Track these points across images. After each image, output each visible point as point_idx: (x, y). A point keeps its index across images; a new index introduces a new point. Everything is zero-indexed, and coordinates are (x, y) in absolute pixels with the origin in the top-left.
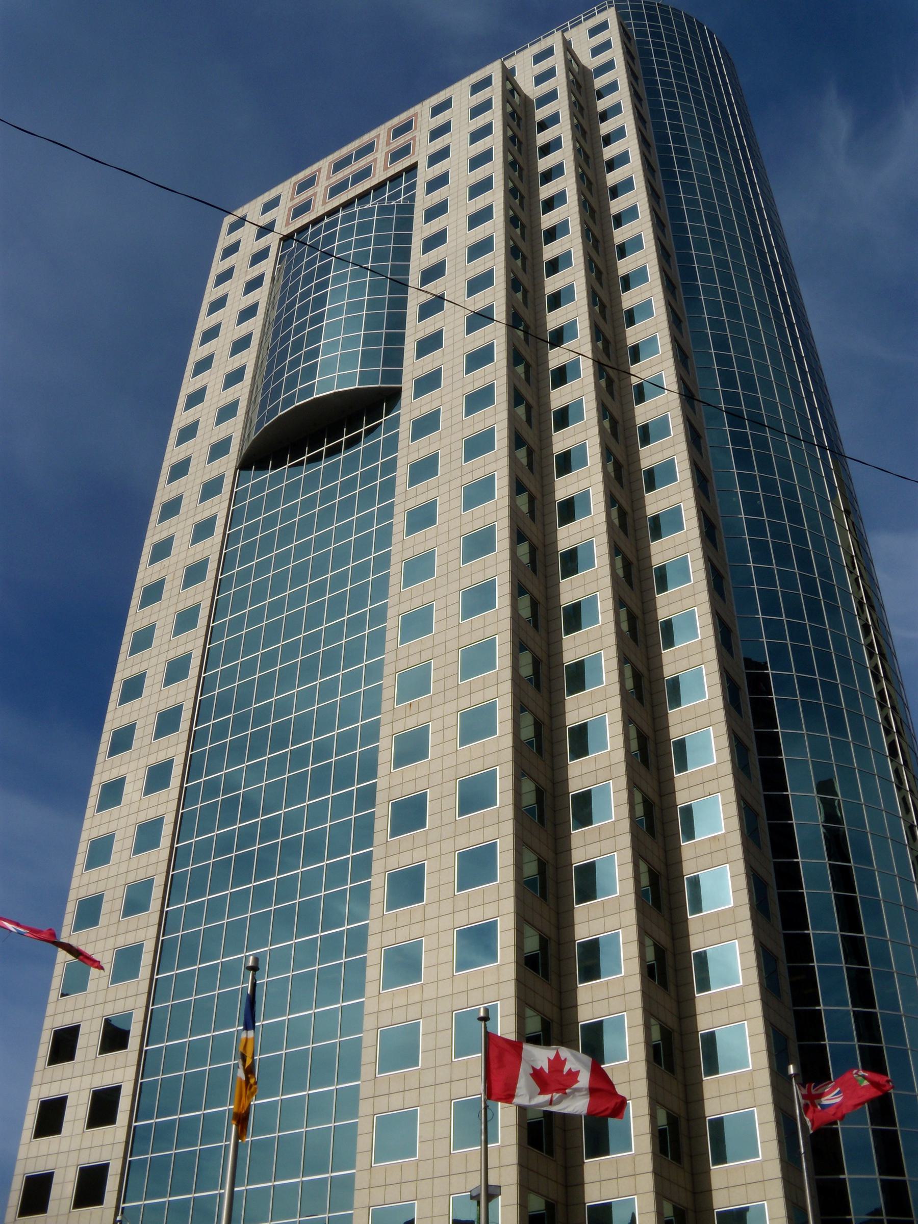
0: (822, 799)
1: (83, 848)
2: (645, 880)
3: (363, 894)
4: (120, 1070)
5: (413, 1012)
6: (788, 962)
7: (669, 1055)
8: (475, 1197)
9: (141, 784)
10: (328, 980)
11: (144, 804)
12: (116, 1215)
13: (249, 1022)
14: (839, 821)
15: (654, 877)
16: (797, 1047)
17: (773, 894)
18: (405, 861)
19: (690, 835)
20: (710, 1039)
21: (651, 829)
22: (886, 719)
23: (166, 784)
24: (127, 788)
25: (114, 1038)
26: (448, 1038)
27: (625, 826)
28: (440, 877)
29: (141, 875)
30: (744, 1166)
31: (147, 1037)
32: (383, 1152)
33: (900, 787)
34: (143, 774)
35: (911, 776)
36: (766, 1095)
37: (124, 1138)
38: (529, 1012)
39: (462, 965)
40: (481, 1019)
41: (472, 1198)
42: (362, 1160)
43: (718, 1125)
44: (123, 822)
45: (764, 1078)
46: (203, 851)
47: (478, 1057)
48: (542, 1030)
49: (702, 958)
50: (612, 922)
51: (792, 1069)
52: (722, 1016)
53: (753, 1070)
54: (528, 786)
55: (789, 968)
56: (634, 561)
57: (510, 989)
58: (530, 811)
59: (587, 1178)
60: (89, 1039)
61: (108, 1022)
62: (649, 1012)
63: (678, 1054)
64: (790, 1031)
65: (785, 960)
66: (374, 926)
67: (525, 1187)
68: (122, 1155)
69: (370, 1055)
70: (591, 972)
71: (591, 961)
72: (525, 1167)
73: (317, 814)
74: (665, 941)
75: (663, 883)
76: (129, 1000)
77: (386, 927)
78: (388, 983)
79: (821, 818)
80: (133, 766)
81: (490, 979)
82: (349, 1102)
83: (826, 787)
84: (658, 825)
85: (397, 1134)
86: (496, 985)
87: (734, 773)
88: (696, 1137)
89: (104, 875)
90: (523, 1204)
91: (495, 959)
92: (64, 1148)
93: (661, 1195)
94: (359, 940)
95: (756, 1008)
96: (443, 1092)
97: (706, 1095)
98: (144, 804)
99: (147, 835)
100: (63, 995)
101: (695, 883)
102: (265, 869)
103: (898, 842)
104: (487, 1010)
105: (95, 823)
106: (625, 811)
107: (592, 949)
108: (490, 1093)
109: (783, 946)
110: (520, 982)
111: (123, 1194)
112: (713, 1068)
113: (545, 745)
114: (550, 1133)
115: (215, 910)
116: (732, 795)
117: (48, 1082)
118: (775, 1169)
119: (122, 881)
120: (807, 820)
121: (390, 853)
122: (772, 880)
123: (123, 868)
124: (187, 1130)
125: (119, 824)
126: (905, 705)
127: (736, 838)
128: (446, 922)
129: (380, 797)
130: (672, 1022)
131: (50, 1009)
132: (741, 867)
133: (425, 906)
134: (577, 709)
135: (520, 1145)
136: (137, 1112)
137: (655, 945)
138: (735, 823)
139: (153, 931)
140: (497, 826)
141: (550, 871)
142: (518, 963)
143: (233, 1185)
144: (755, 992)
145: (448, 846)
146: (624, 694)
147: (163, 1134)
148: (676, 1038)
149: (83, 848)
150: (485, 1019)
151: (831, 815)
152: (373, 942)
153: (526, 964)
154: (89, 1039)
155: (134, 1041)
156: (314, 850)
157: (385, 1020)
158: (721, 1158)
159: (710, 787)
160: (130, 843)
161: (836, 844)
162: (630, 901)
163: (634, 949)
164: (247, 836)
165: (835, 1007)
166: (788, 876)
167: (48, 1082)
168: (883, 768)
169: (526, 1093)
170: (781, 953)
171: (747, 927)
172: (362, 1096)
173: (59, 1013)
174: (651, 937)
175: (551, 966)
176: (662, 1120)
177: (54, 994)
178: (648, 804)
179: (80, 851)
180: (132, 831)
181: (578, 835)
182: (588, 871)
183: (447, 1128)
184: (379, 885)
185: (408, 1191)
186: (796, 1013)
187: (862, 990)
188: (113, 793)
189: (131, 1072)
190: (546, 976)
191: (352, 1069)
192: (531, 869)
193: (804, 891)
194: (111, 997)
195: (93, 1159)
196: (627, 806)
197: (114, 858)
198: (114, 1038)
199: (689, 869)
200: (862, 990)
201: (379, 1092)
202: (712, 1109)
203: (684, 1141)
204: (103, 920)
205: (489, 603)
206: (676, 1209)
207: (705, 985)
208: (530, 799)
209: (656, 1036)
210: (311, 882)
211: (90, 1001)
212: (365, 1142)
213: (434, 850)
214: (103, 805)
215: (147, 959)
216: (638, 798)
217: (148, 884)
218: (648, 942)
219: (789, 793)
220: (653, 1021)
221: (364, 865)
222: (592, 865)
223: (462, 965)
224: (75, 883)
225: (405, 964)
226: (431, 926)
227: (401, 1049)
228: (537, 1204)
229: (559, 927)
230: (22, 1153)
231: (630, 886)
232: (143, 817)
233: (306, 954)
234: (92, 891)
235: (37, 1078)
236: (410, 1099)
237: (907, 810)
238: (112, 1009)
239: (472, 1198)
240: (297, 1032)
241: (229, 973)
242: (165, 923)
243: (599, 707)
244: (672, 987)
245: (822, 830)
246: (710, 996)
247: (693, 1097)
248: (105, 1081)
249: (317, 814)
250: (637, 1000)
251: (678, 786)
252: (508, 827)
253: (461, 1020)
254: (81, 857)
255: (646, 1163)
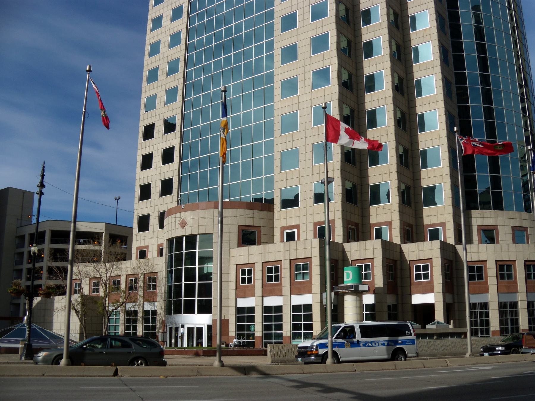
0: (474, 13)
1: (145, 74)
2: (394, 48)
3: (271, 57)
4: (173, 140)
5: (295, 108)
6: (456, 84)
7: (404, 123)
8: (323, 183)
9: (170, 17)
10: (258, 96)
11: (172, 26)
12: (178, 198)
13: (225, 114)
14: (482, 24)
15: (398, 47)
16: (458, 118)
17: (451, 55)
18: (288, 43)
19: (414, 28)
20: (422, 117)
21: (397, 26)
22: (526, 123)
23: (181, 16)
24: (164, 20)
25: (169, 127)
26: (310, 118)
27: (385, 24)
28: (304, 49)
29: (174, 57)
30: (434, 169)
31: (183, 126)
32: (285, 166)
33: (510, 9)
34: (170, 13)
35: (515, 4)
36: (445, 140)
37: (178, 167)
38: (344, 106)
39: (315, 86)
40: (323, 108)
41: (322, 183)
42: (276, 170)
43: (424, 152)
44: (163, 35)
45: (444, 133)
46: (200, 44)
47: (322, 126)
48: (346, 15)
49: (419, 82)
50: (380, 67)
51: (455, 129)
52: (426, 107)
53: (433, 60)
54: (342, 7)
55: (456, 87)
56: (400, 13)
57: (336, 96)
58: (343, 18)
59: (370, 174)
60: (159, 129)
61: (166, 121)
62: (396, 105)
63: (408, 123)
64: (456, 114)
65: (448, 20)
66: (276, 71)
67: (344, 179)
68: (186, 26)
69: (277, 127)
70: (371, 88)
71: (371, 83)
72: (343, 170)
73: (249, 24)
74: (403, 75)
75: (402, 50)
76: (174, 111)
77: (281, 72)
78: (283, 96)
79: (473, 22)
80: (165, 9)
81: (327, 92)
82: (270, 147)
83: (476, 8)
84: (403, 55)
85: (290, 158)
86: (330, 94)
87: (441, 66)
88: (415, 158)
89: (150, 174)
90: (343, 185)
91: (329, 83)
92: (154, 173)
93: (400, 181)
94: (270, 78)
95: (442, 104)
96: (309, 141)
97: (420, 140)
98: (172, 26)
99: (175, 40)
100: (146, 112)
101: (416, 50)
102: (228, 49)
103: (507, 34)
104: (325, 104)
105: (151, 37)
106: (385, 18)
107: (371, 78)
108: (327, 139)
109: (454, 78)
110: (340, 93)
111: (180, 190)
112: (423, 129)
113: (351, 20)
114: (354, 157)
115: (207, 69)
116: (433, 11)
117: (144, 147)
118: (447, 171)
119: (166, 60)
120: (467, 23)
121: (282, 39)
122: (450, 49)
123: (166, 55)
124: (203, 163)
125: (161, 35)
126: (523, 23)
127: (435, 30)
128: (308, 68)
129: (276, 15)
130: (405, 109)
131: (141, 118)
132: (436, 43)
133: (298, 62)
134: (369, 67)
135: (342, 161)
136: (181, 157)
137: (398, 77)
138: (435, 23)
139: (181, 80)
140: (330, 58)
141: (352, 45)
142: (339, 85)
143: (223, 163)
144: (441, 97)
145: (307, 35)
146: (392, 55)
147: (194, 165)
148: (405, 82)
149: (145, 74)
150: (325, 108)
151: (478, 20)
152: (276, 78)
153: (343, 85)
154: (159, 129)
155: (178, 128)
156: (248, 39)
157: (283, 111)
158: (425, 166)
159: (423, 7)
160: (167, 43)
161: (479, 34)
162: (388, 58)
163: (389, 78)
164: (218, 37)
165: (475, 105)
166: (458, 47)
167: (144, 147)
168: (518, 119)
169: (344, 139)
170: (453, 81)
171: (438, 69)
172: (275, 143)
173: (145, 119)
174: (397, 73)
175: (354, 85)
176: (401, 151)
177: (142, 111)
178: (396, 15)
179: (134, 221)
180: (168, 38)
181: (364, 29)
182: (369, 45)
183: (310, 155)
184: (277, 53)
185: (296, 182)
186: (459, 107)
187: (487, 98)
188: (158, 22)
189: (178, 140)
190: (351, 90)
191: (270, 132)
192: (344, 44)
193: (464, 54)
194: (166, 110)
195: (166, 177)
196: (386, 15)
197: (161, 51)
198: (169, 127)
199: (414, 43)
200: (487, 98)
201: (282, 142)
202: (422, 146)
203: (412, 197)
204: (159, 78)
205: (327, 81)
206: (406, 186)
207: (420, 94)
208: (343, 13)
209: (399, 115)
210: (248, 54)
211: (158, 113)
212: (277, 163)
213: (301, 37)
214: (154, 28)
215: (180, 93)
216: (391, 12)
217: (175, 89)
218: (396, 75)
219: (466, 71)
220: (397, 109)
221: (270, 46)
222: (373, 75)
223: (315, 86)
224: (145, 63)
225: (290, 87)
226: (301, 70)
227: (290, 123)
228: (349, 185)
229: (355, 37)
230: (137, 177)
231: (388, 51)
232: (172, 32)
233: (247, 85)
234: (153, 66)
235: (139, 146)
236: (295, 144)
237: (512, 19)
238: (167, 116)
239: (322, 183)
240: (246, 119)
241: (215, 96)
242: (186, 77)
243: (380, 67)
244: (406, 95)
245: (473, 27)
246: (422, 98)
247: (414, 141)
248: (167, 145)
249: (249, 24)
250: (390, 100)
251: (415, 70)
252: (334, 26)
253: (315, 110)
254: (143, 106)
255: (394, 168)
